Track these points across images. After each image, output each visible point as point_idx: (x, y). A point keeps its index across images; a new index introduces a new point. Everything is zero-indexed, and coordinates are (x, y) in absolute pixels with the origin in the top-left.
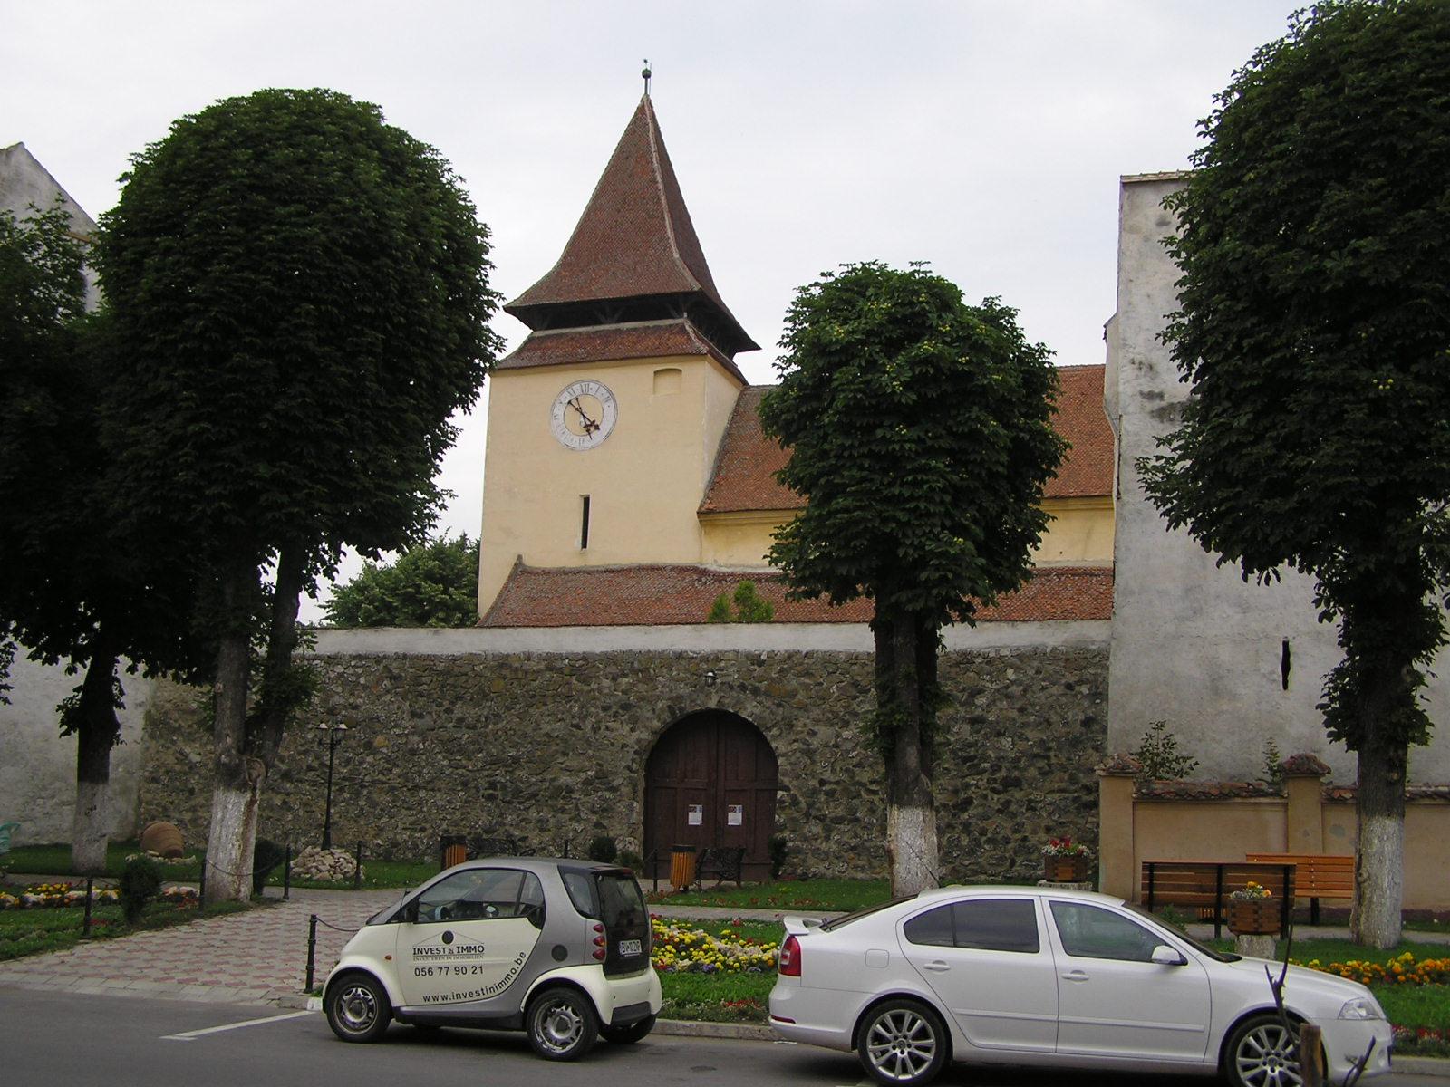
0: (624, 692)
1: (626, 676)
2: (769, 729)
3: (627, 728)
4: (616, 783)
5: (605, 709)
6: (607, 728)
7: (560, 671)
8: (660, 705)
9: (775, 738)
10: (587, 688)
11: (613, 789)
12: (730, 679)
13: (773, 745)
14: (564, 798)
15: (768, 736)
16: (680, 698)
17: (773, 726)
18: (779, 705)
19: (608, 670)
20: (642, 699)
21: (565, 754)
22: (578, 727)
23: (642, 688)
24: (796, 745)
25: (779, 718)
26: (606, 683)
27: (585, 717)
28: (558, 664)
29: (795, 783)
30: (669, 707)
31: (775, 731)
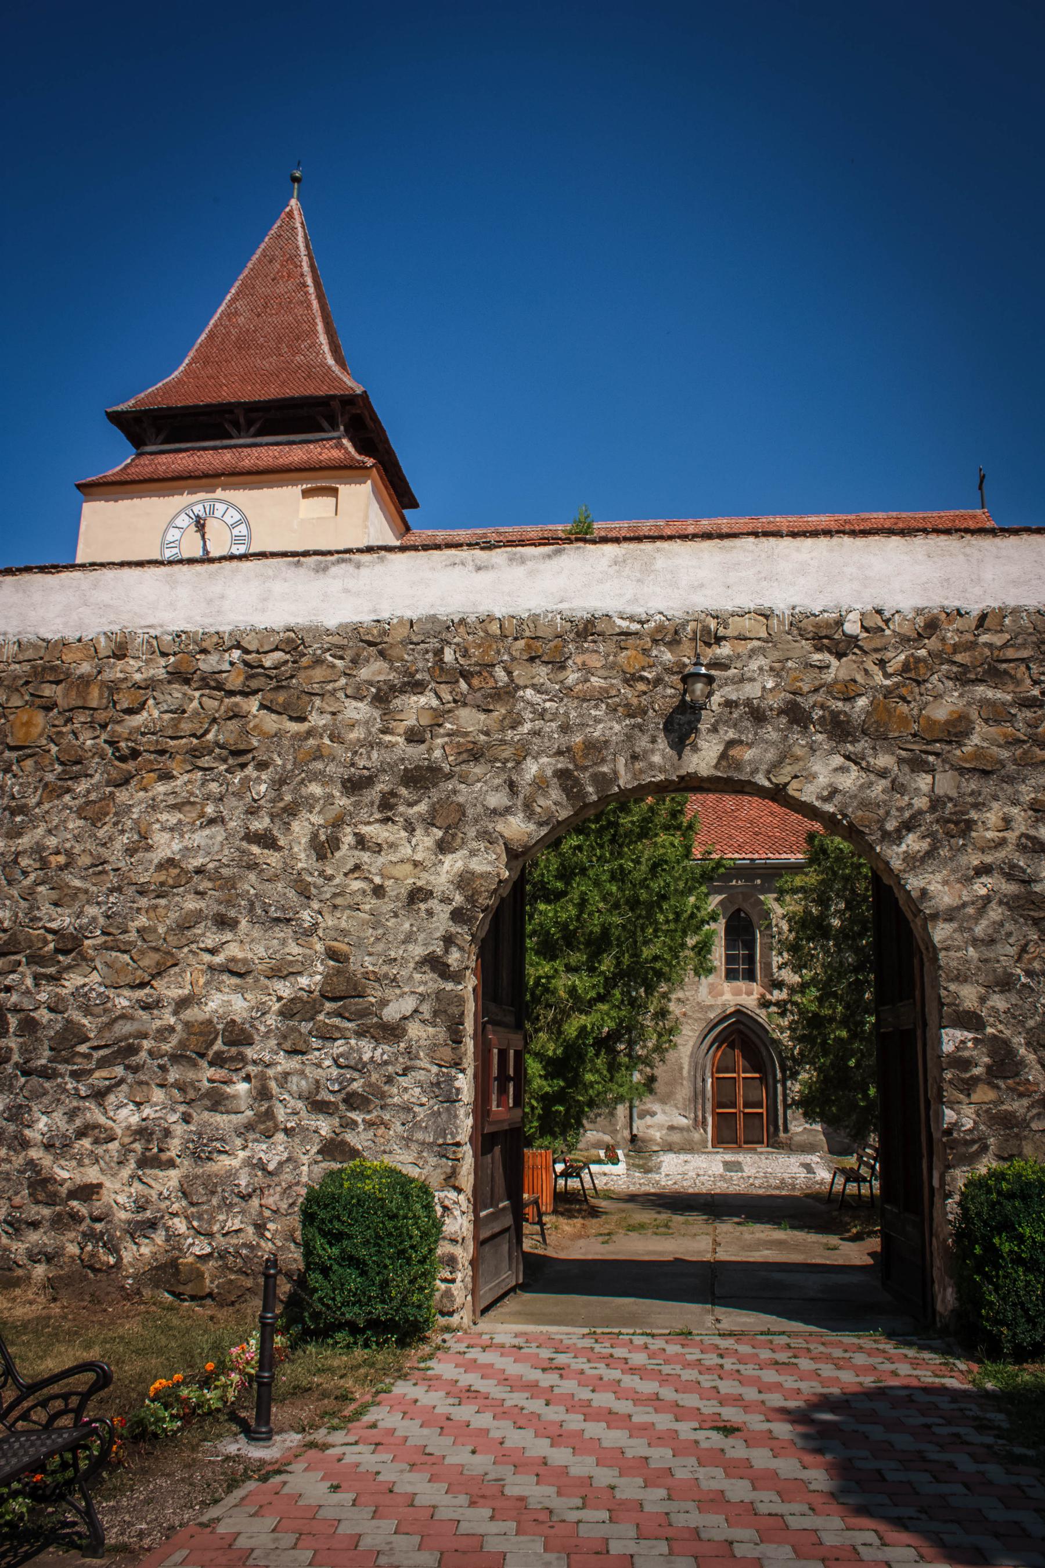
0: (414, 737)
1: (418, 687)
2: (896, 837)
3: (425, 841)
4: (391, 1013)
5: (354, 785)
6: (361, 842)
7: (212, 683)
8: (532, 768)
9: (915, 862)
10: (294, 727)
11: (392, 1032)
12: (751, 691)
13: (914, 883)
14: (218, 1061)
15: (895, 855)
16: (594, 748)
17: (908, 826)
18: (917, 765)
19: (364, 673)
20: (476, 754)
21: (224, 923)
22: (267, 841)
23: (470, 719)
24: (980, 888)
25: (921, 803)
26: (358, 710)
27: (292, 811)
28: (208, 663)
29: (999, 1002)
30: (562, 775)
31: (913, 843)
